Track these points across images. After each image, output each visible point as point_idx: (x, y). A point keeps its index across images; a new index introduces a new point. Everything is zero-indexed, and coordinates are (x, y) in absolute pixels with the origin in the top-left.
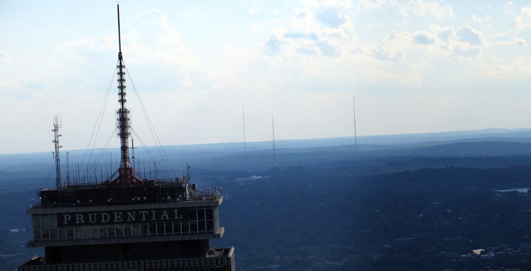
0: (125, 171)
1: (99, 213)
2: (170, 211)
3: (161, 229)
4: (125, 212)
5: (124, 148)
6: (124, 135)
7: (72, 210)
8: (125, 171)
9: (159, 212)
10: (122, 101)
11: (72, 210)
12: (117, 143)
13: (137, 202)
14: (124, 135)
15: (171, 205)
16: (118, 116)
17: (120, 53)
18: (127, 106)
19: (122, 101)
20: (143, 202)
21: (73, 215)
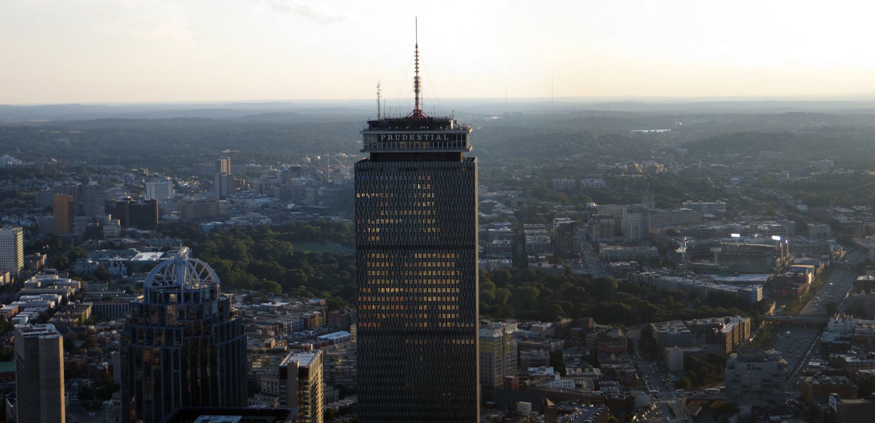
0: (417, 112)
1: (401, 135)
2: (442, 135)
3: (436, 145)
4: (416, 135)
5: (417, 99)
6: (417, 91)
7: (386, 132)
8: (417, 112)
9: (435, 135)
10: (417, 72)
11: (386, 132)
12: (414, 95)
13: (423, 129)
14: (417, 91)
15: (442, 132)
16: (414, 80)
17: (417, 78)
18: (419, 74)
19: (417, 72)
20: (426, 129)
21: (387, 135)
